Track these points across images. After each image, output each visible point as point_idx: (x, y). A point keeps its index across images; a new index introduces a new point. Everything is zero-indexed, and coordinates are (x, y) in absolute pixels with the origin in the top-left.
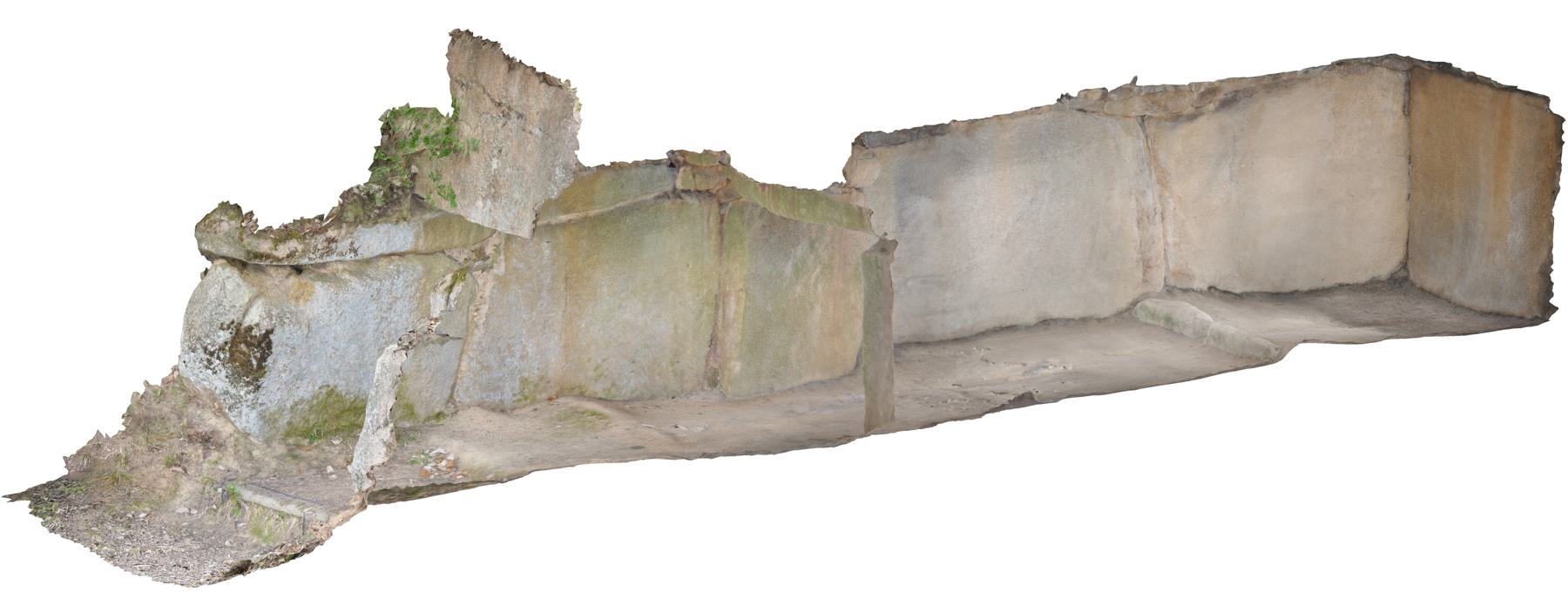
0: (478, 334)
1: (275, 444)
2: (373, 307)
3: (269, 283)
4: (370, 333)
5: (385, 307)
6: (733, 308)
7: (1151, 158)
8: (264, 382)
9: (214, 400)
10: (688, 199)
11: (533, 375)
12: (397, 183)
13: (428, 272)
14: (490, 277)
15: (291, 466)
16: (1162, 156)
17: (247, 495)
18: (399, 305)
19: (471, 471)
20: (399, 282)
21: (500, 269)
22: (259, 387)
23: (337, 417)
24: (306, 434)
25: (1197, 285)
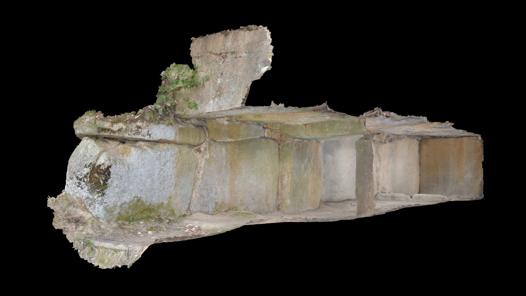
0: (199, 182)
1: (112, 223)
2: (157, 163)
3: (109, 147)
4: (156, 175)
5: (162, 164)
6: (286, 180)
8: (107, 192)
9: (82, 203)
11: (220, 201)
12: (169, 105)
13: (180, 152)
14: (203, 159)
15: (120, 231)
16: (380, 153)
17: (97, 243)
18: (168, 164)
19: (208, 230)
20: (169, 153)
22: (104, 194)
23: (142, 212)
24: (127, 219)
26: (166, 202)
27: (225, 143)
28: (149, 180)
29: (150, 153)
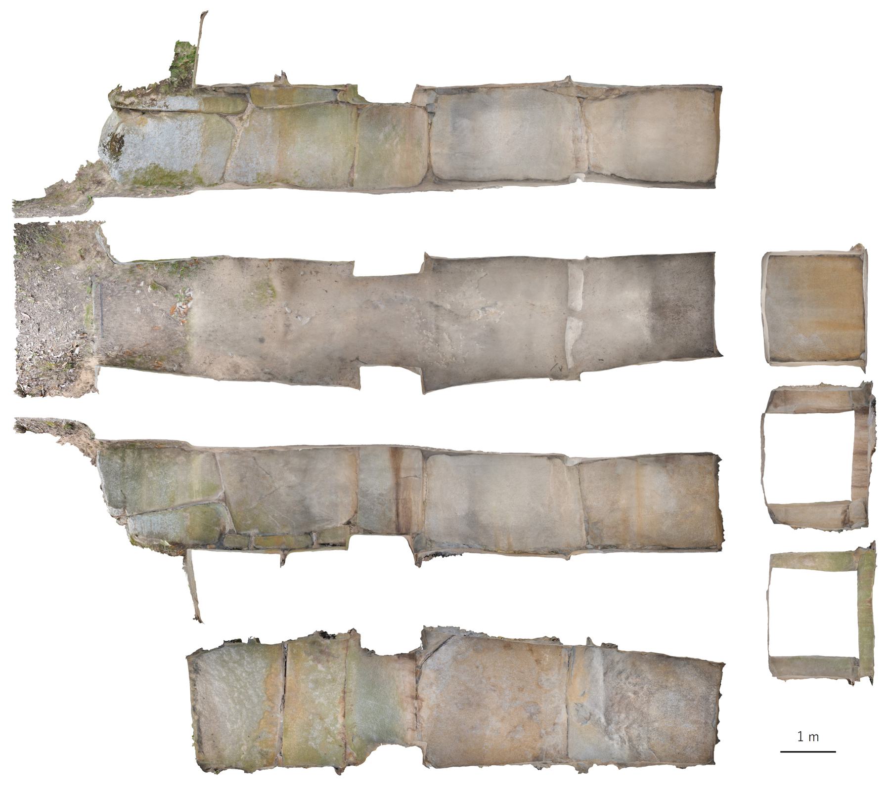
0: (236, 151)
2: (178, 132)
7: (582, 115)
8: (121, 158)
10: (341, 105)
11: (263, 172)
13: (207, 121)
16: (587, 114)
18: (192, 134)
20: (192, 123)
21: (247, 125)
25: (604, 172)
26: (190, 170)
27: (273, 110)
28: (167, 148)
29: (168, 123)
